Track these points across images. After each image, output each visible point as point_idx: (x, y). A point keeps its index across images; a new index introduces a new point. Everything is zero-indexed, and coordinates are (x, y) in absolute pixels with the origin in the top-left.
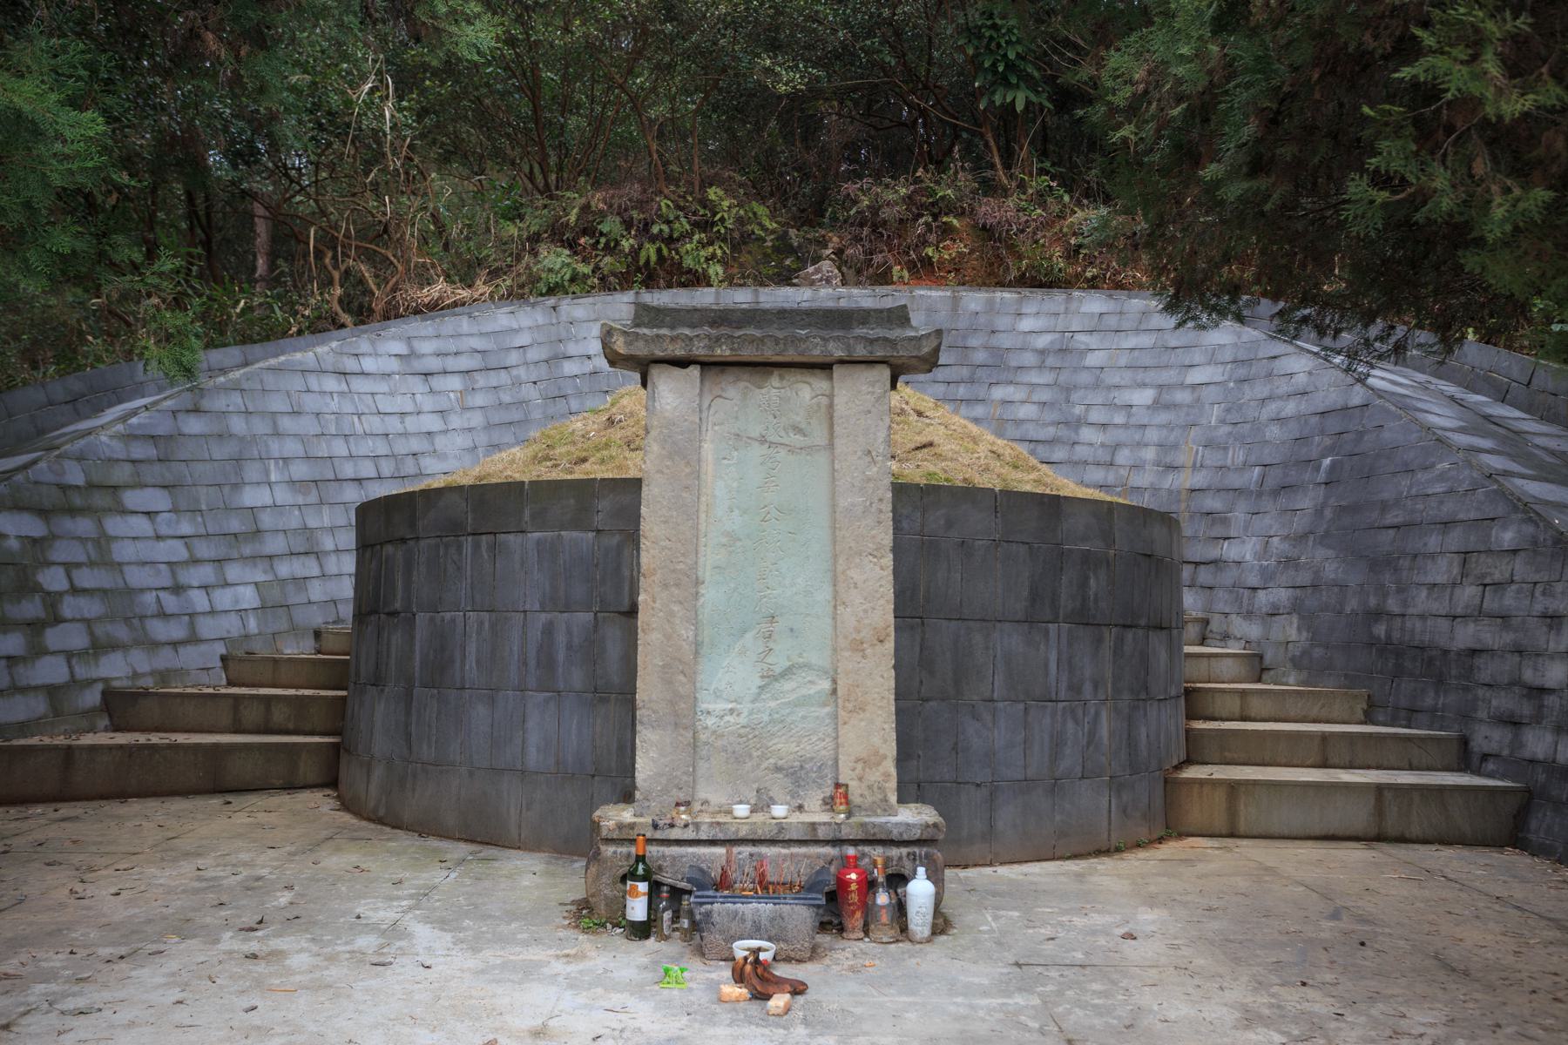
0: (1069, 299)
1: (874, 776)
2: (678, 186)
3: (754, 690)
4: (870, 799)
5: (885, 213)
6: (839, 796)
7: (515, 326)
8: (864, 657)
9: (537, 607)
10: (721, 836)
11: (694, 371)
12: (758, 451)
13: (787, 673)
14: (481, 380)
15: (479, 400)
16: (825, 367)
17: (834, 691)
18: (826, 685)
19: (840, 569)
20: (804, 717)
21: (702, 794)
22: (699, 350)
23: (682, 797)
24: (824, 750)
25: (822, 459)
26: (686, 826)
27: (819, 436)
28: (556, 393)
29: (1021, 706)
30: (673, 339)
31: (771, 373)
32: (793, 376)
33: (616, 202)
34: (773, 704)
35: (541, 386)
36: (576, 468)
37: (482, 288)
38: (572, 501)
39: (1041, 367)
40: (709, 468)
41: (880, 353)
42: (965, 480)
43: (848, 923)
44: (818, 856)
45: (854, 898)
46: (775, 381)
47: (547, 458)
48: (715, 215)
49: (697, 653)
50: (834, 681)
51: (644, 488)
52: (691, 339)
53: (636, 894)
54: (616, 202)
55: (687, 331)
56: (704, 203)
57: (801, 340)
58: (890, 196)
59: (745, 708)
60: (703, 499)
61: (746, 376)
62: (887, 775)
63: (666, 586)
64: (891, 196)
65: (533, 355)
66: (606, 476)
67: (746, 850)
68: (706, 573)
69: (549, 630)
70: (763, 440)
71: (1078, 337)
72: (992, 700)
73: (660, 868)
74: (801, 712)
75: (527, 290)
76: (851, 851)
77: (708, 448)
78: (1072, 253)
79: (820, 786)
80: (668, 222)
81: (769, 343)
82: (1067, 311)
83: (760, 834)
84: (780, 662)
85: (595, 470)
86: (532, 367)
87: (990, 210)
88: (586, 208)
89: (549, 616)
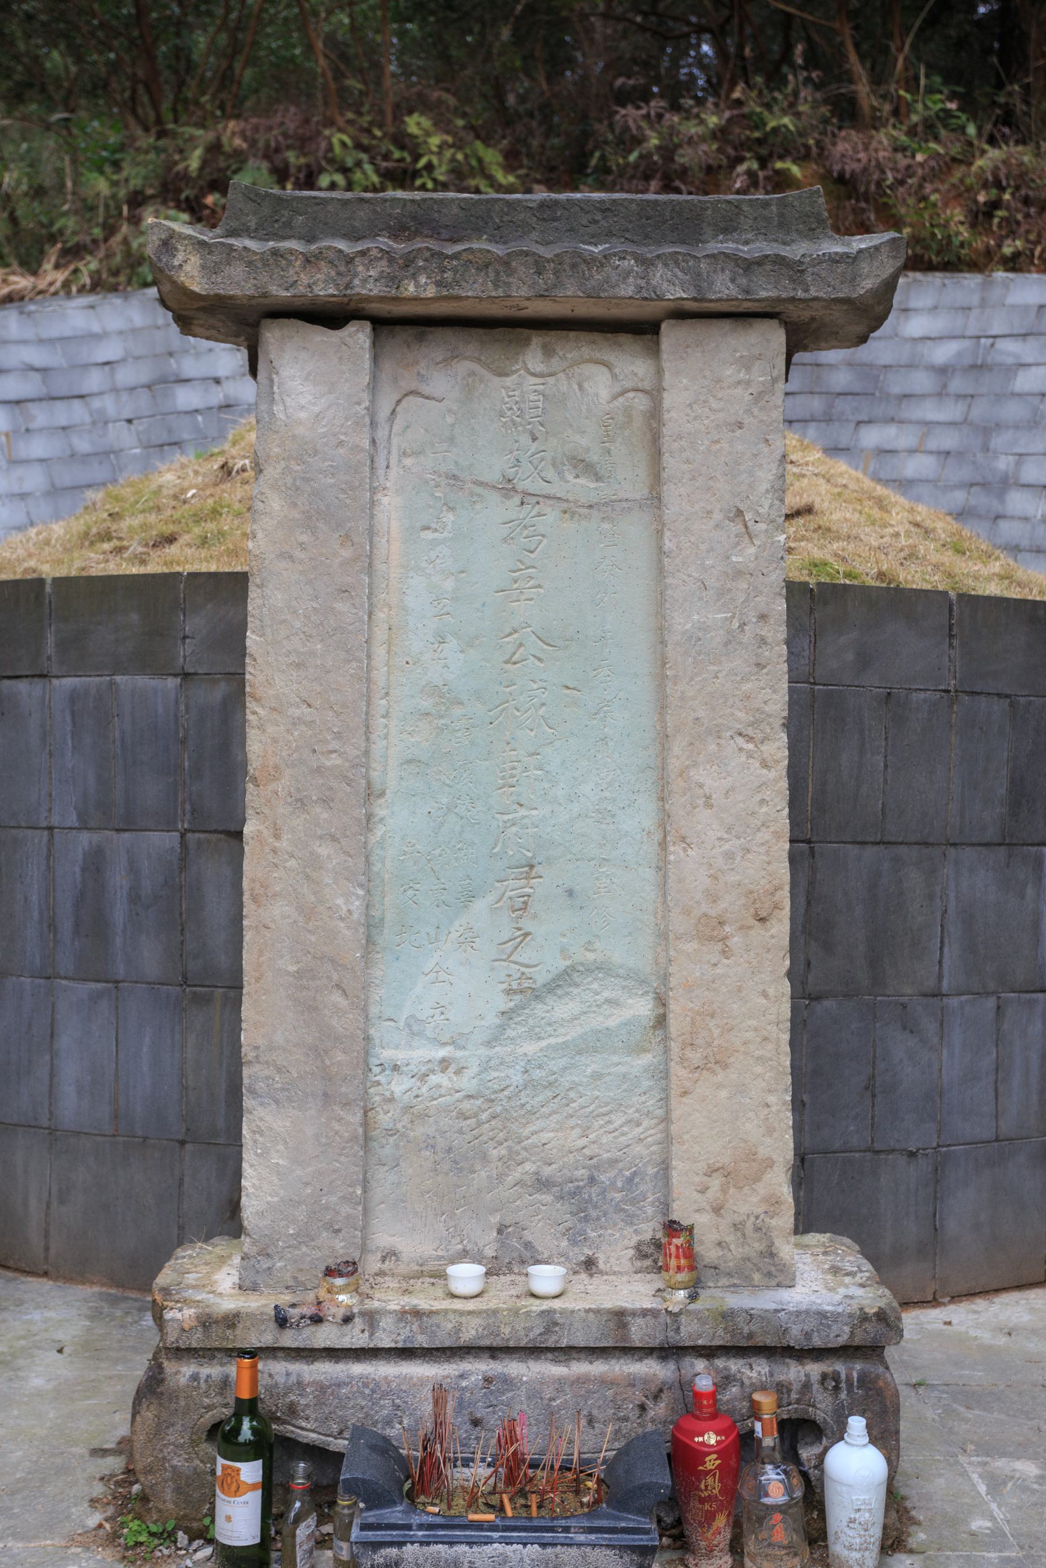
0: (986, 286)
1: (746, 1204)
2: (360, 114)
3: (492, 1019)
4: (737, 1252)
5: (685, 157)
6: (671, 1246)
7: (96, 328)
8: (725, 953)
9: (73, 820)
10: (422, 1341)
11: (358, 336)
12: (497, 512)
13: (562, 982)
14: (40, 416)
15: (37, 447)
16: (642, 329)
17: (661, 1021)
18: (642, 1008)
19: (674, 764)
20: (597, 1076)
21: (383, 1238)
22: (368, 284)
23: (340, 1248)
24: (640, 1143)
25: (635, 530)
26: (347, 1320)
27: (629, 479)
28: (165, 438)
29: (991, 1003)
30: (309, 261)
31: (527, 342)
32: (574, 349)
33: (262, 139)
34: (531, 1048)
35: (139, 426)
36: (154, 554)
37: (52, 276)
38: (135, 617)
39: (941, 395)
40: (392, 548)
41: (766, 291)
42: (881, 575)
43: (700, 1539)
44: (632, 1382)
45: (712, 1485)
46: (533, 358)
47: (106, 536)
48: (417, 157)
49: (370, 941)
50: (661, 1001)
51: (253, 593)
52: (350, 260)
53: (237, 1489)
54: (262, 139)
55: (342, 245)
56: (401, 140)
57: (591, 261)
58: (693, 129)
59: (473, 1056)
60: (381, 615)
61: (471, 349)
62: (772, 1201)
63: (301, 803)
64: (693, 129)
65: (125, 376)
66: (204, 568)
67: (478, 1368)
68: (389, 774)
69: (96, 863)
70: (508, 488)
71: (1002, 345)
72: (938, 994)
73: (292, 1410)
74: (592, 1065)
75: (122, 278)
76: (703, 1377)
77: (391, 507)
78: (980, 217)
79: (630, 1219)
80: (345, 170)
81: (523, 270)
82: (983, 303)
83: (507, 1334)
84: (545, 960)
85: (187, 558)
86: (125, 396)
87: (848, 149)
88: (214, 149)
89: (96, 837)
